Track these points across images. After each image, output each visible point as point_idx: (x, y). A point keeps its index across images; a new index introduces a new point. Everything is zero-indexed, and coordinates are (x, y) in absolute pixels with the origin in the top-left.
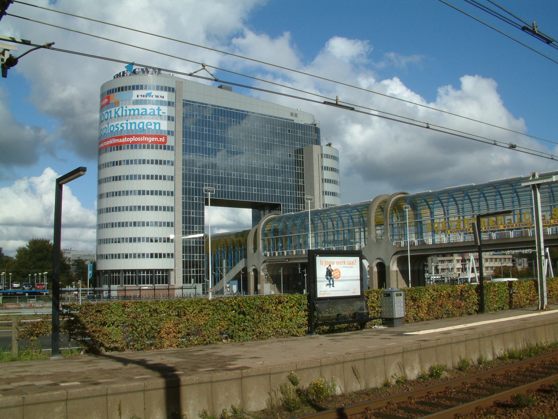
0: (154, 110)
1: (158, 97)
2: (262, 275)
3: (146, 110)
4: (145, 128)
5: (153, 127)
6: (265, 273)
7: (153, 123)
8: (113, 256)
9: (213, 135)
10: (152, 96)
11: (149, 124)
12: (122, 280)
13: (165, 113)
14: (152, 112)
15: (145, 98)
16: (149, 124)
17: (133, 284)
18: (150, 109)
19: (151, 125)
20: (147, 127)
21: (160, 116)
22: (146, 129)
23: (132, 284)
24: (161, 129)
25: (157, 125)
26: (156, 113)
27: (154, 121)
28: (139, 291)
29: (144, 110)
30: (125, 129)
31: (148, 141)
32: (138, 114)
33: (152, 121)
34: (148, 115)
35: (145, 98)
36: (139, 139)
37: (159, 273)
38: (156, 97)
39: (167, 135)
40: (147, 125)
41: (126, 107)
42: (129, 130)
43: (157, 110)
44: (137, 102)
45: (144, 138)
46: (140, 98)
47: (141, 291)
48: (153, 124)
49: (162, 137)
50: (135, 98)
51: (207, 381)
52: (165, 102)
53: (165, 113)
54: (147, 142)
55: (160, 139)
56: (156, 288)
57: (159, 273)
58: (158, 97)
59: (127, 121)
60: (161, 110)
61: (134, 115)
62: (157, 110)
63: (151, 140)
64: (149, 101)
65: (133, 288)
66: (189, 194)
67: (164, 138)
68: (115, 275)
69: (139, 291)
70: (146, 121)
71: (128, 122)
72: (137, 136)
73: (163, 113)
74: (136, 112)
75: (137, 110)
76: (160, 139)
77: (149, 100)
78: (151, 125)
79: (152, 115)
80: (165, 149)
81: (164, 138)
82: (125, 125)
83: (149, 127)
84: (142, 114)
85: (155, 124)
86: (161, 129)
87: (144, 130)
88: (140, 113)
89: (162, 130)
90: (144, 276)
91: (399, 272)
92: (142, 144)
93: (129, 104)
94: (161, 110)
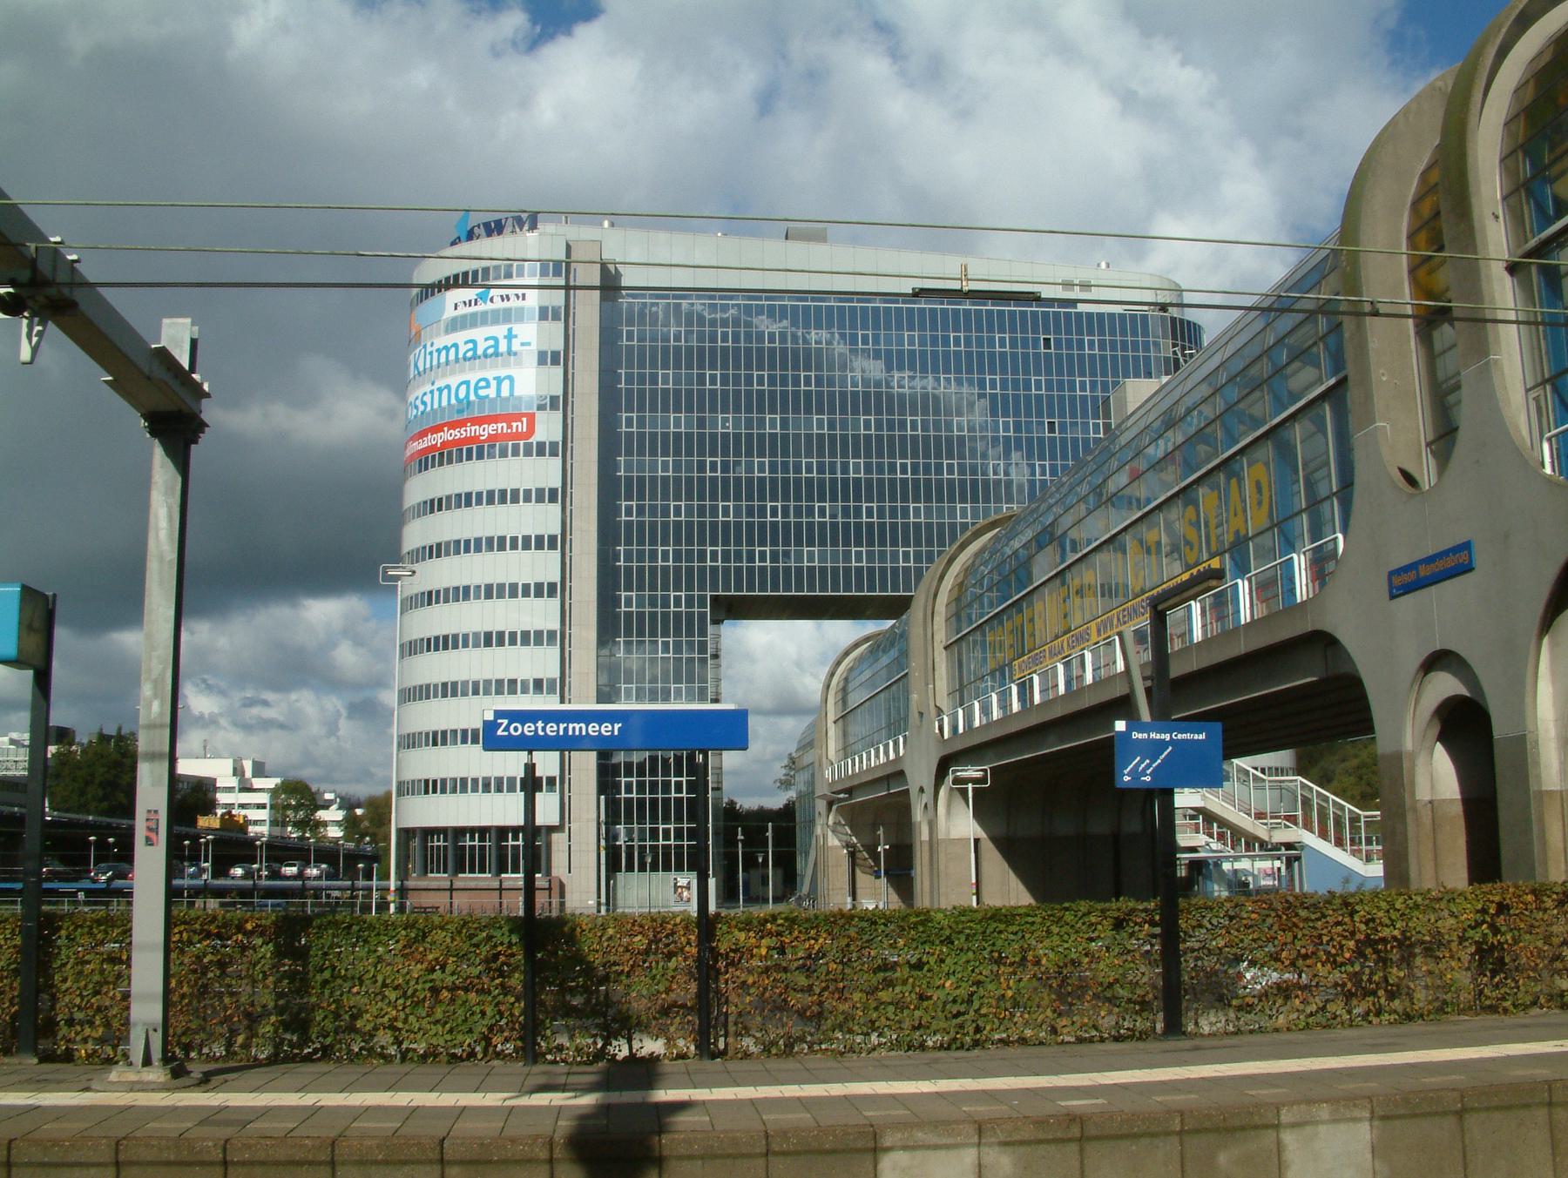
0: (496, 339)
1: (508, 300)
2: (832, 847)
3: (474, 342)
4: (472, 397)
5: (492, 393)
6: (845, 838)
7: (495, 379)
8: (431, 786)
9: (1019, 395)
10: (492, 300)
11: (483, 384)
12: (491, 859)
13: (529, 344)
14: (492, 346)
15: (473, 309)
16: (483, 384)
17: (485, 872)
18: (486, 339)
19: (488, 386)
20: (476, 394)
21: (515, 354)
22: (474, 402)
23: (482, 871)
24: (516, 393)
25: (506, 385)
26: (503, 348)
27: (496, 373)
28: (449, 892)
29: (492, 342)
30: (429, 409)
31: (481, 435)
32: (457, 360)
33: (490, 374)
34: (479, 357)
35: (473, 309)
36: (457, 434)
37: (472, 839)
38: (503, 300)
39: (535, 410)
40: (477, 388)
41: (432, 345)
42: (437, 410)
43: (505, 337)
44: (456, 325)
45: (468, 429)
46: (463, 310)
47: (454, 893)
48: (494, 384)
49: (518, 417)
50: (449, 313)
51: (1284, 1159)
52: (531, 310)
53: (529, 344)
54: (474, 439)
55: (514, 424)
56: (505, 885)
57: (472, 839)
58: (508, 300)
59: (433, 384)
60: (516, 336)
61: (447, 363)
62: (505, 337)
63: (486, 433)
64: (485, 313)
65: (483, 884)
66: (653, 587)
67: (524, 420)
68: (511, 843)
69: (449, 892)
70: (473, 377)
71: (435, 387)
72: (453, 425)
73: (522, 344)
74: (452, 356)
75: (453, 349)
76: (514, 424)
77: (516, 309)
78: (488, 386)
79: (491, 355)
80: (528, 453)
81: (524, 420)
82: (427, 399)
83: (482, 393)
84: (465, 359)
85: (499, 380)
86: (516, 393)
87: (469, 403)
88: (480, 352)
89: (520, 398)
90: (472, 848)
91: (988, 847)
92: (465, 448)
93: (438, 335)
94: (516, 336)
